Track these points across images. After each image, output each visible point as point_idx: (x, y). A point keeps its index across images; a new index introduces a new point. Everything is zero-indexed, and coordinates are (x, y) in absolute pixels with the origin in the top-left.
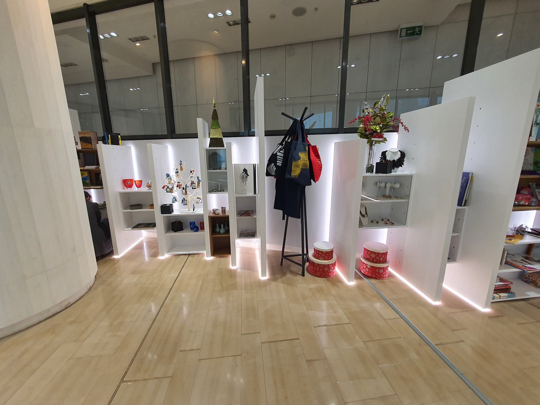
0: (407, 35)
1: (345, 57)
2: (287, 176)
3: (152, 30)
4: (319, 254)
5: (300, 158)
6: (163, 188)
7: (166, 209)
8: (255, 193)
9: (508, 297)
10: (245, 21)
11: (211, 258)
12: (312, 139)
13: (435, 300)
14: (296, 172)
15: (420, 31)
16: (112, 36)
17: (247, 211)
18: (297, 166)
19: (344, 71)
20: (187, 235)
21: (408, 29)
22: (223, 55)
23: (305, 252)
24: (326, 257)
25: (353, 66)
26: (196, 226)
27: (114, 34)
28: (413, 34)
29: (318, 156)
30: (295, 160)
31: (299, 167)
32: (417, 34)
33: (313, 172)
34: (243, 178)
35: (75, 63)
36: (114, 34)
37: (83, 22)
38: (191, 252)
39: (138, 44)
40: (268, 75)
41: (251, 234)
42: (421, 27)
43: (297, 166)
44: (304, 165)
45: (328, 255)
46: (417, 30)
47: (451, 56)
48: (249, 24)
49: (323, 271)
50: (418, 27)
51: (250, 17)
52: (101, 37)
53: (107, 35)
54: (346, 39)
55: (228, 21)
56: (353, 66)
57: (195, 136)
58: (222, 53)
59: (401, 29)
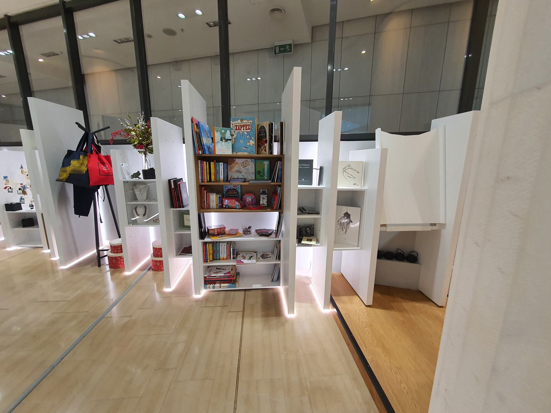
0: (280, 52)
1: (331, 59)
3: (62, 45)
6: (6, 188)
9: (229, 287)
10: (223, 22)
15: (290, 48)
16: (91, 37)
19: (330, 76)
21: (280, 47)
22: (121, 70)
24: (115, 251)
25: (346, 69)
27: (92, 34)
28: (285, 51)
31: (66, 172)
32: (288, 52)
35: (3, 75)
36: (92, 34)
37: (58, 22)
38: (36, 246)
39: (41, 60)
40: (249, 80)
42: (290, 45)
46: (288, 47)
47: (343, 69)
48: (229, 25)
50: (288, 45)
51: (230, 17)
52: (80, 37)
53: (86, 36)
54: (449, 22)
55: (207, 21)
56: (346, 69)
57: (20, 144)
58: (120, 68)
59: (275, 47)
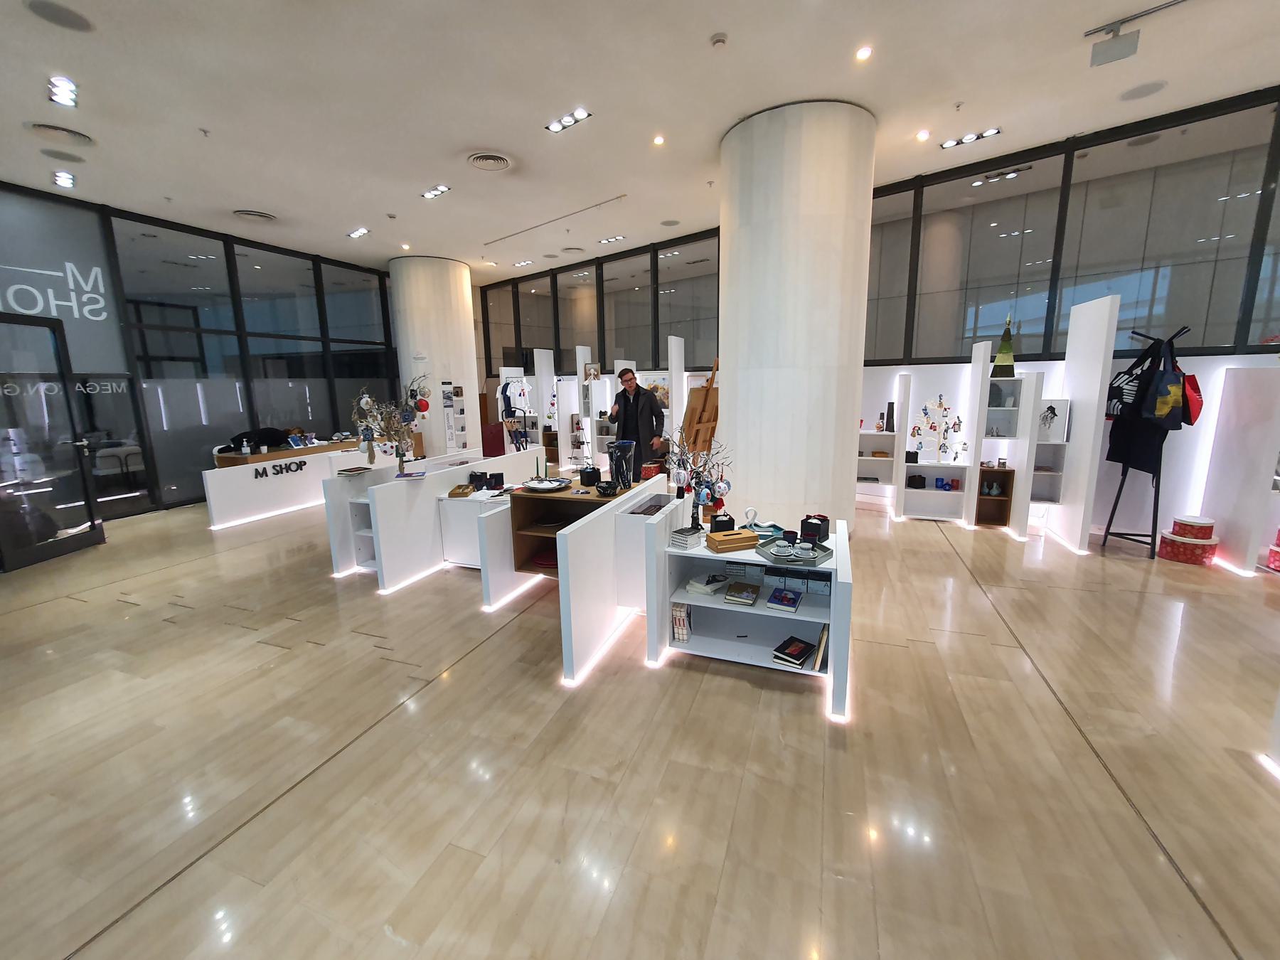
2: (1146, 415)
4: (1181, 528)
5: (1169, 393)
7: (912, 457)
8: (1068, 440)
11: (973, 527)
12: (1187, 365)
13: (31, 293)
14: (1162, 410)
16: (223, 933)
17: (1049, 462)
18: (1165, 403)
20: (930, 496)
23: (135, 333)
26: (950, 482)
29: (1196, 389)
30: (1162, 395)
33: (1187, 412)
34: (1044, 419)
41: (1052, 498)
43: (1165, 403)
44: (1176, 401)
45: (1205, 531)
49: (1193, 553)
